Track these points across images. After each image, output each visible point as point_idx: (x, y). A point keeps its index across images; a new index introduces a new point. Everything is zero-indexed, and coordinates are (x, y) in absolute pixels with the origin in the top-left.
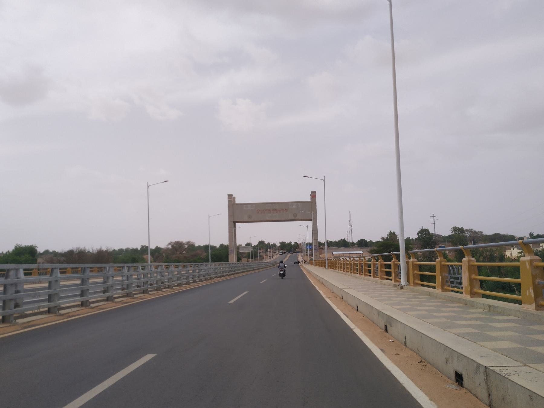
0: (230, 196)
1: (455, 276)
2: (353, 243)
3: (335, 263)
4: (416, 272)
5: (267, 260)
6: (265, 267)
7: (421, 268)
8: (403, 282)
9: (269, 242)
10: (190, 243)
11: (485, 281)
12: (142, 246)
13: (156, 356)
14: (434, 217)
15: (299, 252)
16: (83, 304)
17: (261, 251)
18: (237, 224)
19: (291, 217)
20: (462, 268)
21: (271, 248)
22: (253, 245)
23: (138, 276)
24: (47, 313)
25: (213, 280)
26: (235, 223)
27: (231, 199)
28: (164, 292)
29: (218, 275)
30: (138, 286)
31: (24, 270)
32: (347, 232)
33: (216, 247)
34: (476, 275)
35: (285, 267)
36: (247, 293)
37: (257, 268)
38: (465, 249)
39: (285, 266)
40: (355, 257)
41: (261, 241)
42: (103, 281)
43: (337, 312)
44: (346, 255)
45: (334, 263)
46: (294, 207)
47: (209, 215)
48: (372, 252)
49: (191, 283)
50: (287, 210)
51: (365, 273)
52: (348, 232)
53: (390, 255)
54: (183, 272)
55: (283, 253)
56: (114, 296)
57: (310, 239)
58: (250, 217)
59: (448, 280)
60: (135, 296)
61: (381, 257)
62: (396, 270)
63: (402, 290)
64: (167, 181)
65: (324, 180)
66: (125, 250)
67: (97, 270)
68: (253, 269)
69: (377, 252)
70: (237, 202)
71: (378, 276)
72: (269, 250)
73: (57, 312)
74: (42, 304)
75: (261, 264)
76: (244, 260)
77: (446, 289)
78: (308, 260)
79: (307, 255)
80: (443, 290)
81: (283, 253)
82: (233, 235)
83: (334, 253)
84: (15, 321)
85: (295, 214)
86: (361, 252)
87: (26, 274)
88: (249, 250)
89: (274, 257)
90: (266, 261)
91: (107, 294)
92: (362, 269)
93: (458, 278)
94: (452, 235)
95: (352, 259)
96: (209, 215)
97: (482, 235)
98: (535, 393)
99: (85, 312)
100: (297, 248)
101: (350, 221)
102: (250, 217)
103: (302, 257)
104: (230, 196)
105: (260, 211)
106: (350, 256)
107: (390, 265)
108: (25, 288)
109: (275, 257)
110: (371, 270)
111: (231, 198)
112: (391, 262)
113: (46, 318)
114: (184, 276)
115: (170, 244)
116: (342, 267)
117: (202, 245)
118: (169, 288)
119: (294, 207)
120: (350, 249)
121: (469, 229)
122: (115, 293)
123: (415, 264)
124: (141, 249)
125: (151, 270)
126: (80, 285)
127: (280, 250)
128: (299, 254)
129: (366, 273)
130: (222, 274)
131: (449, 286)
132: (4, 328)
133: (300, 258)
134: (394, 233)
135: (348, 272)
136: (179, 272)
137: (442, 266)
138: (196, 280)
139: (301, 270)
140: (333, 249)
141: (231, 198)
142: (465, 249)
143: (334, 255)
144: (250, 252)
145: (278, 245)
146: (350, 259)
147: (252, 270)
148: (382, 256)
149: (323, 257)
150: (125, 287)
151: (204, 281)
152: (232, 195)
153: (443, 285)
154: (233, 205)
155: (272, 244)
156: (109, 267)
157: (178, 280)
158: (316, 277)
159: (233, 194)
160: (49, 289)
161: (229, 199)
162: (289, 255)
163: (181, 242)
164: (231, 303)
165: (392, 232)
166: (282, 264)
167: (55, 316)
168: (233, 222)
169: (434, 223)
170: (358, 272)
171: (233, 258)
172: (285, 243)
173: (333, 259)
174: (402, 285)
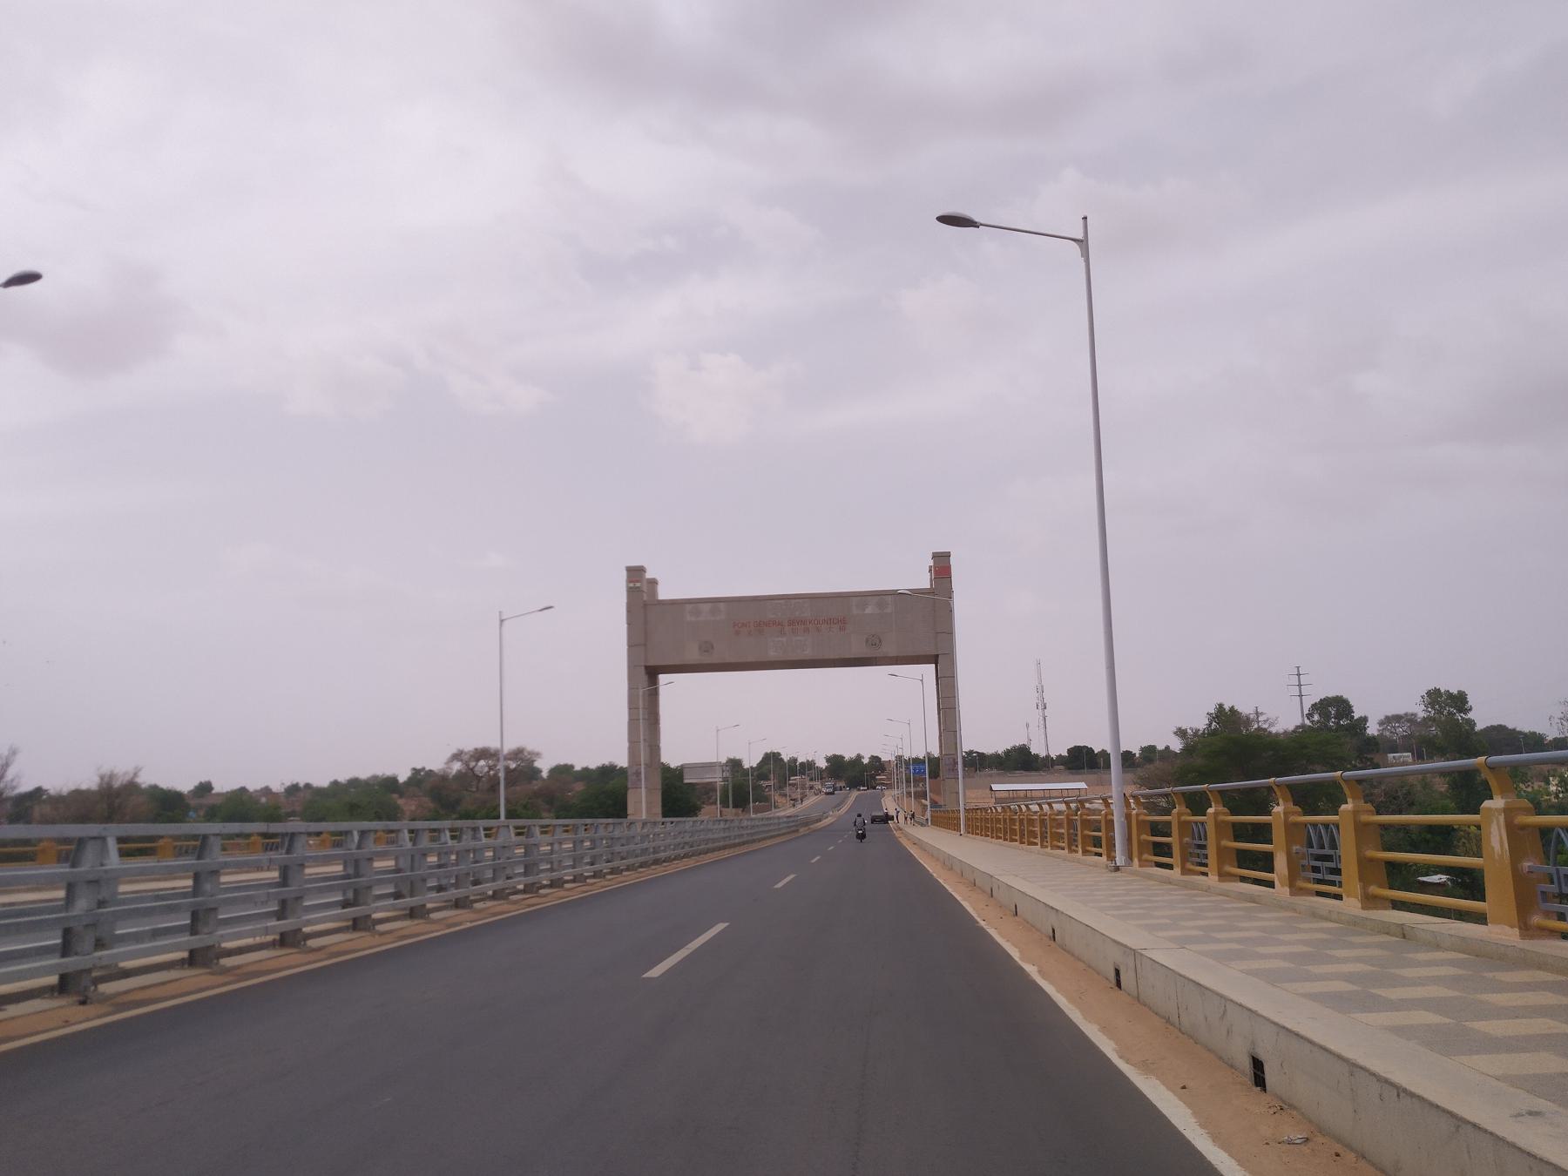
0: (635, 573)
2: (1048, 756)
4: (1144, 837)
7: (1240, 832)
8: (1120, 859)
11: (1406, 864)
12: (414, 769)
14: (1299, 675)
16: (195, 959)
18: (661, 677)
20: (1338, 829)
23: (439, 855)
24: (56, 994)
26: (653, 673)
27: (638, 585)
28: (382, 934)
29: (652, 856)
30: (440, 889)
31: (121, 840)
42: (393, 868)
44: (1034, 794)
45: (1005, 820)
46: (869, 610)
49: (567, 882)
50: (842, 623)
53: (1203, 793)
55: (835, 789)
57: (923, 742)
58: (707, 648)
59: (1305, 862)
60: (380, 928)
61: (1182, 799)
62: (1072, 831)
64: (551, 607)
65: (1083, 243)
67: (175, 847)
71: (1203, 869)
73: (93, 988)
77: (1301, 889)
80: (1296, 891)
81: (835, 789)
83: (995, 787)
84: (96, 990)
86: (1082, 785)
87: (124, 854)
89: (807, 803)
91: (408, 901)
92: (1076, 835)
93: (1328, 858)
95: (1046, 807)
99: (291, 962)
100: (879, 775)
101: (1041, 690)
102: (707, 648)
103: (897, 799)
104: (635, 573)
105: (744, 625)
109: (811, 800)
110: (1101, 837)
111: (638, 583)
112: (1477, 812)
113: (54, 1009)
114: (381, 882)
115: (457, 756)
116: (1015, 829)
117: (593, 766)
118: (360, 930)
119: (869, 610)
120: (1041, 775)
121: (1406, 714)
127: (827, 779)
129: (1146, 856)
130: (652, 856)
131: (1308, 880)
132: (292, 956)
133: (889, 805)
135: (1036, 844)
137: (1290, 828)
138: (424, 906)
140: (991, 776)
141: (638, 581)
142: (1346, 781)
145: (822, 764)
146: (1041, 808)
150: (350, 895)
151: (609, 877)
153: (1184, 860)
154: (645, 605)
156: (363, 833)
157: (526, 874)
160: (194, 897)
161: (631, 585)
162: (855, 793)
164: (723, 922)
166: (859, 820)
168: (647, 668)
169: (1301, 696)
171: (643, 802)
174: (1118, 864)
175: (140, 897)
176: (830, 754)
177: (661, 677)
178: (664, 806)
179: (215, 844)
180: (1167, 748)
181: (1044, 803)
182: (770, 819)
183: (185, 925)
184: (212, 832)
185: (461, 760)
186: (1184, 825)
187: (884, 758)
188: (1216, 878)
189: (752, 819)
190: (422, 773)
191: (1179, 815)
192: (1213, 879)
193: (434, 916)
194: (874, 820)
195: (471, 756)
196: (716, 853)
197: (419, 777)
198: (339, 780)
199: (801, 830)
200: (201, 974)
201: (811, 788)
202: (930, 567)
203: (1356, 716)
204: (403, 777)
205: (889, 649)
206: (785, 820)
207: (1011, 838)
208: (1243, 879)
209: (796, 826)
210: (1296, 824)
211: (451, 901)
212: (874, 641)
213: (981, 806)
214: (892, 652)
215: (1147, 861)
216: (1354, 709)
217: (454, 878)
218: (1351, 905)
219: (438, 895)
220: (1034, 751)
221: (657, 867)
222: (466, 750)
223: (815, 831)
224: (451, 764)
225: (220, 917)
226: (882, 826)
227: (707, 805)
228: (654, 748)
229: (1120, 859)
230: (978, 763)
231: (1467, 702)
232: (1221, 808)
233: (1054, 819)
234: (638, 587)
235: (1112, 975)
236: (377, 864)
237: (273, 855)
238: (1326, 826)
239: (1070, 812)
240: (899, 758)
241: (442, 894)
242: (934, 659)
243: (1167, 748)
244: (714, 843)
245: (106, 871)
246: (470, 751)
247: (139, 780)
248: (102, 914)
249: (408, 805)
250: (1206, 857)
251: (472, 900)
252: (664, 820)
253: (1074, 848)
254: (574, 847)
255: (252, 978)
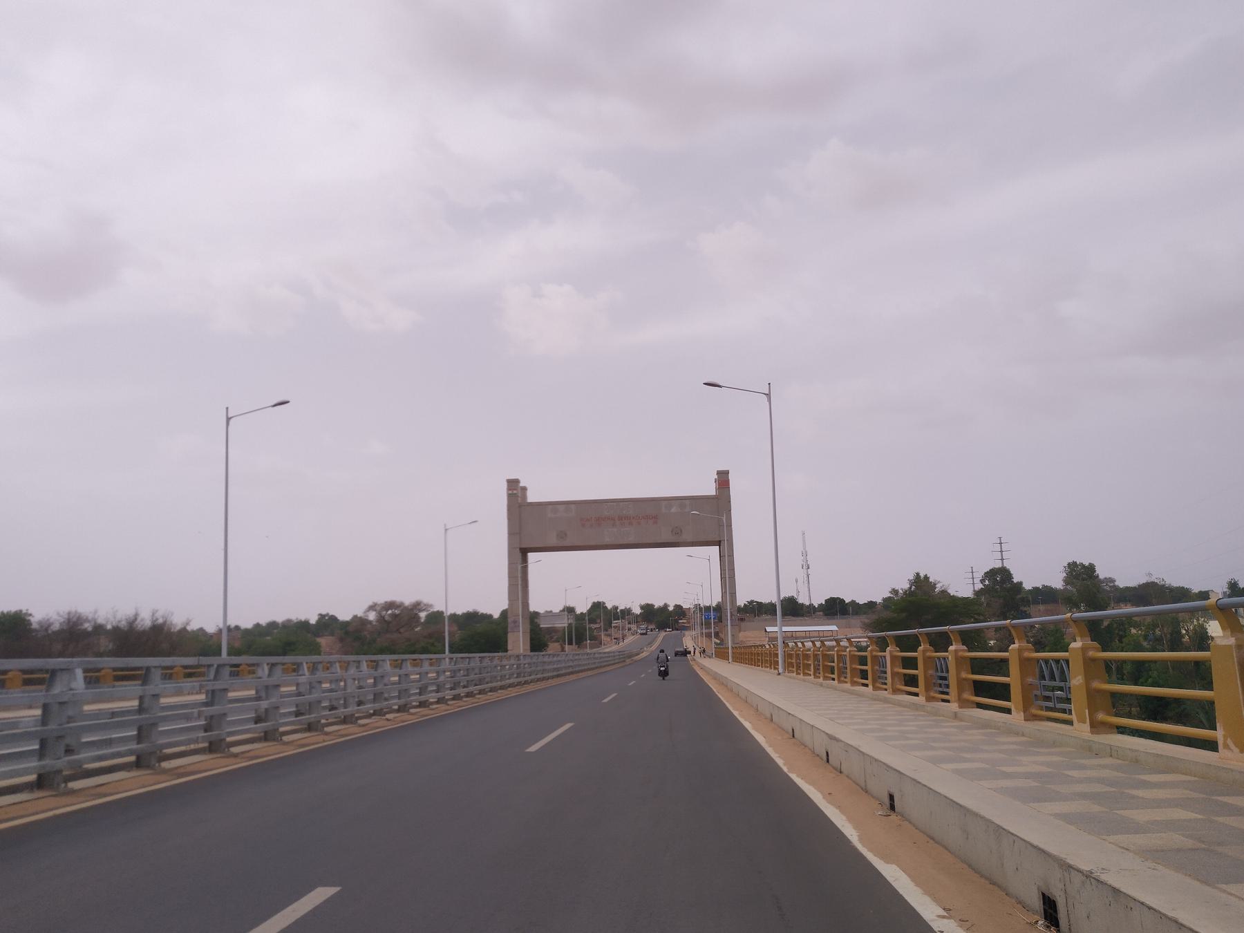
0: (513, 484)
1: (1053, 683)
2: (811, 605)
3: (803, 655)
4: (964, 675)
5: (610, 648)
6: (597, 665)
8: (781, 670)
9: (617, 604)
10: (422, 605)
12: (320, 615)
13: (339, 892)
14: (1001, 543)
15: (686, 628)
17: (597, 626)
18: (532, 556)
19: (666, 536)
21: (619, 620)
22: (578, 611)
24: (35, 790)
25: (460, 703)
26: (524, 552)
27: (515, 492)
28: (412, 714)
30: (332, 708)
32: (797, 581)
33: (491, 616)
34: (968, 673)
35: (668, 660)
36: (572, 727)
37: (571, 670)
38: (951, 632)
39: (667, 658)
40: (826, 641)
41: (596, 601)
43: (826, 812)
44: (798, 634)
45: (770, 653)
46: (673, 510)
47: (445, 525)
48: (878, 625)
50: (655, 518)
51: (852, 677)
52: (800, 581)
53: (915, 636)
54: (412, 677)
56: (282, 729)
57: (712, 597)
58: (562, 535)
59: (1038, 693)
62: (841, 665)
63: (779, 676)
64: (287, 402)
65: (768, 395)
66: (280, 626)
68: (555, 673)
69: (892, 625)
70: (532, 497)
71: (884, 687)
72: (615, 623)
73: (226, 750)
74: (193, 735)
75: (586, 657)
76: (553, 647)
78: (711, 649)
79: (709, 636)
82: (520, 582)
83: (768, 629)
84: (66, 786)
85: (677, 527)
86: (834, 628)
88: (563, 623)
90: (607, 650)
92: (819, 665)
94: (974, 599)
95: (818, 644)
96: (445, 525)
97: (1115, 586)
98: (976, 815)
99: (216, 765)
100: (681, 619)
101: (805, 554)
102: (562, 535)
103: (694, 639)
104: (513, 484)
106: (807, 636)
107: (916, 658)
108: (86, 711)
109: (630, 639)
110: (867, 671)
111: (515, 489)
112: (1006, 650)
115: (372, 608)
116: (792, 663)
119: (673, 510)
120: (805, 620)
122: (283, 723)
123: (961, 657)
124: (318, 622)
125: (260, 678)
126: (206, 704)
127: (641, 623)
128: (687, 633)
131: (1041, 708)
133: (688, 642)
134: (926, 578)
136: (423, 675)
137: (1024, 663)
138: (460, 694)
139: (695, 671)
141: (515, 490)
142: (1014, 626)
143: (770, 636)
144: (565, 627)
145: (637, 611)
146: (814, 645)
147: (553, 677)
148: (928, 634)
149: (744, 640)
152: (516, 481)
153: (927, 689)
154: (520, 506)
155: (623, 608)
158: (747, 700)
159: (527, 486)
161: (510, 492)
162: (663, 634)
163: (398, 603)
164: (569, 722)
165: (920, 577)
166: (661, 655)
167: (55, 796)
168: (521, 549)
170: (833, 676)
171: (518, 642)
172: (652, 606)
173: (769, 645)
175: (97, 715)
176: (643, 603)
177: (529, 554)
178: (531, 647)
179: (156, 675)
180: (1021, 583)
181: (817, 641)
182: (600, 653)
183: (36, 750)
184: (154, 665)
185: (376, 610)
186: (927, 660)
187: (685, 606)
188: (1087, 727)
189: (588, 654)
190: (327, 618)
191: (924, 651)
192: (954, 706)
193: (327, 729)
194: (676, 654)
195: (383, 607)
196: (567, 677)
197: (324, 620)
198: (261, 623)
199: (627, 661)
200: (148, 774)
201: (629, 629)
202: (716, 479)
203: (1015, 580)
204: (313, 621)
205: (686, 537)
206: (618, 654)
207: (803, 671)
208: (1122, 730)
209: (624, 658)
210: (1029, 660)
211: (340, 717)
212: (677, 531)
213: (758, 643)
214: (690, 539)
215: (968, 701)
216: (1014, 576)
217: (343, 699)
218: (1082, 730)
219: (255, 726)
220: (800, 601)
221: (502, 691)
222: (379, 603)
223: (636, 661)
224: (368, 613)
225: (160, 729)
226: (683, 658)
227: (551, 642)
228: (526, 604)
229: (781, 670)
230: (757, 610)
231: (1095, 571)
232: (1025, 644)
233: (826, 655)
234: (515, 494)
235: (887, 801)
236: (412, 677)
237: (416, 669)
238: (1057, 661)
239: (816, 649)
240: (697, 607)
241: (258, 725)
242: (719, 543)
243: (1021, 583)
244: (559, 671)
245: (73, 695)
246: (381, 604)
247: (189, 628)
248: (71, 728)
249: (323, 641)
250: (948, 686)
251: (323, 724)
252: (532, 653)
253: (842, 679)
254: (400, 679)
255: (182, 777)
